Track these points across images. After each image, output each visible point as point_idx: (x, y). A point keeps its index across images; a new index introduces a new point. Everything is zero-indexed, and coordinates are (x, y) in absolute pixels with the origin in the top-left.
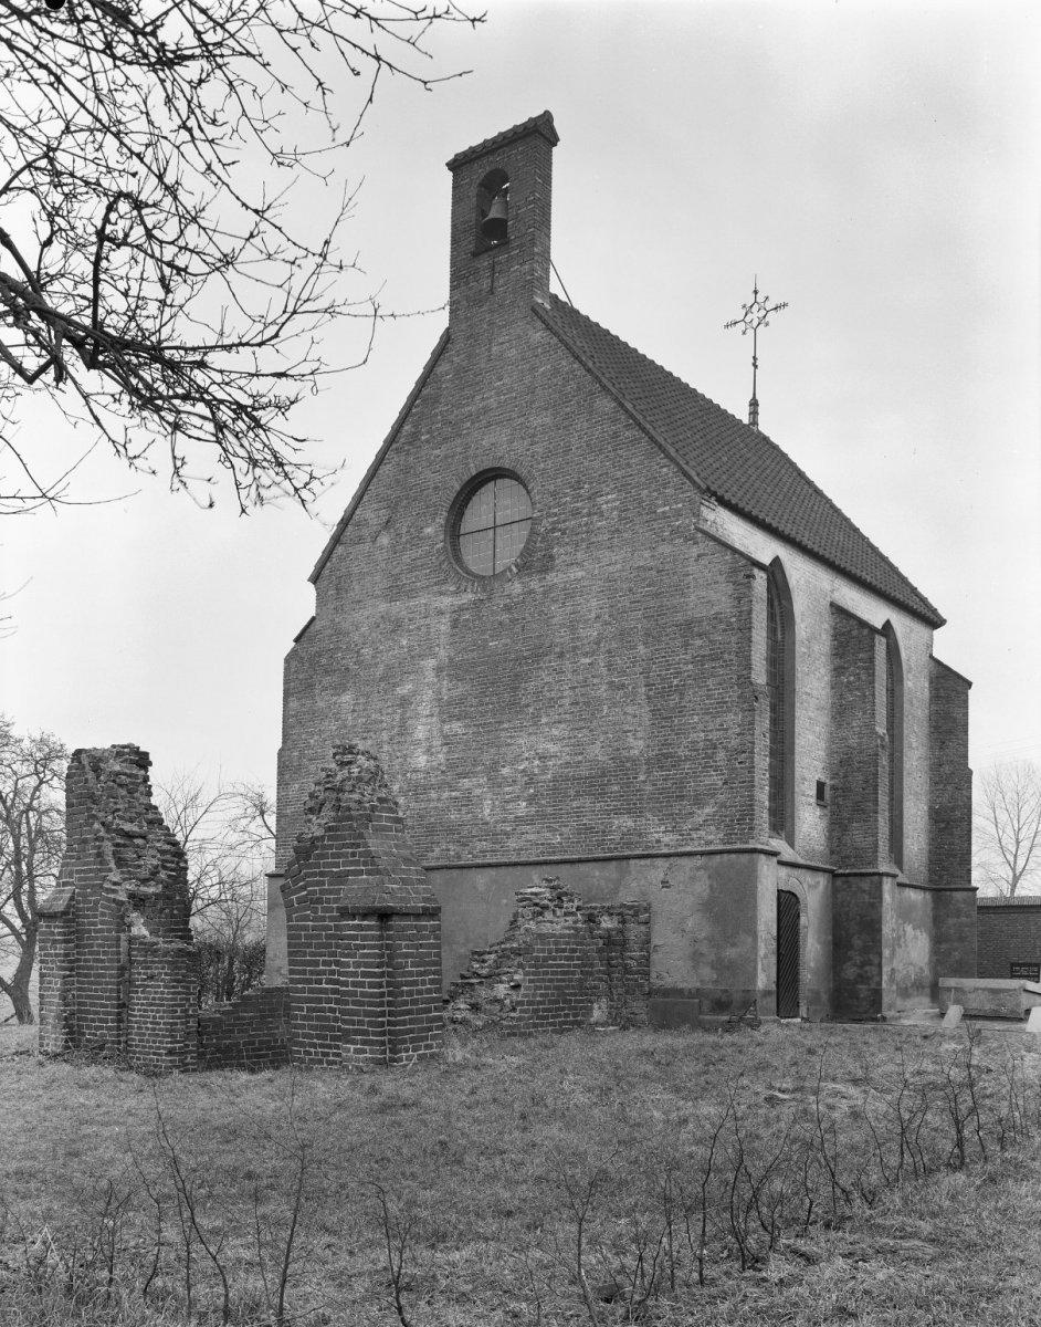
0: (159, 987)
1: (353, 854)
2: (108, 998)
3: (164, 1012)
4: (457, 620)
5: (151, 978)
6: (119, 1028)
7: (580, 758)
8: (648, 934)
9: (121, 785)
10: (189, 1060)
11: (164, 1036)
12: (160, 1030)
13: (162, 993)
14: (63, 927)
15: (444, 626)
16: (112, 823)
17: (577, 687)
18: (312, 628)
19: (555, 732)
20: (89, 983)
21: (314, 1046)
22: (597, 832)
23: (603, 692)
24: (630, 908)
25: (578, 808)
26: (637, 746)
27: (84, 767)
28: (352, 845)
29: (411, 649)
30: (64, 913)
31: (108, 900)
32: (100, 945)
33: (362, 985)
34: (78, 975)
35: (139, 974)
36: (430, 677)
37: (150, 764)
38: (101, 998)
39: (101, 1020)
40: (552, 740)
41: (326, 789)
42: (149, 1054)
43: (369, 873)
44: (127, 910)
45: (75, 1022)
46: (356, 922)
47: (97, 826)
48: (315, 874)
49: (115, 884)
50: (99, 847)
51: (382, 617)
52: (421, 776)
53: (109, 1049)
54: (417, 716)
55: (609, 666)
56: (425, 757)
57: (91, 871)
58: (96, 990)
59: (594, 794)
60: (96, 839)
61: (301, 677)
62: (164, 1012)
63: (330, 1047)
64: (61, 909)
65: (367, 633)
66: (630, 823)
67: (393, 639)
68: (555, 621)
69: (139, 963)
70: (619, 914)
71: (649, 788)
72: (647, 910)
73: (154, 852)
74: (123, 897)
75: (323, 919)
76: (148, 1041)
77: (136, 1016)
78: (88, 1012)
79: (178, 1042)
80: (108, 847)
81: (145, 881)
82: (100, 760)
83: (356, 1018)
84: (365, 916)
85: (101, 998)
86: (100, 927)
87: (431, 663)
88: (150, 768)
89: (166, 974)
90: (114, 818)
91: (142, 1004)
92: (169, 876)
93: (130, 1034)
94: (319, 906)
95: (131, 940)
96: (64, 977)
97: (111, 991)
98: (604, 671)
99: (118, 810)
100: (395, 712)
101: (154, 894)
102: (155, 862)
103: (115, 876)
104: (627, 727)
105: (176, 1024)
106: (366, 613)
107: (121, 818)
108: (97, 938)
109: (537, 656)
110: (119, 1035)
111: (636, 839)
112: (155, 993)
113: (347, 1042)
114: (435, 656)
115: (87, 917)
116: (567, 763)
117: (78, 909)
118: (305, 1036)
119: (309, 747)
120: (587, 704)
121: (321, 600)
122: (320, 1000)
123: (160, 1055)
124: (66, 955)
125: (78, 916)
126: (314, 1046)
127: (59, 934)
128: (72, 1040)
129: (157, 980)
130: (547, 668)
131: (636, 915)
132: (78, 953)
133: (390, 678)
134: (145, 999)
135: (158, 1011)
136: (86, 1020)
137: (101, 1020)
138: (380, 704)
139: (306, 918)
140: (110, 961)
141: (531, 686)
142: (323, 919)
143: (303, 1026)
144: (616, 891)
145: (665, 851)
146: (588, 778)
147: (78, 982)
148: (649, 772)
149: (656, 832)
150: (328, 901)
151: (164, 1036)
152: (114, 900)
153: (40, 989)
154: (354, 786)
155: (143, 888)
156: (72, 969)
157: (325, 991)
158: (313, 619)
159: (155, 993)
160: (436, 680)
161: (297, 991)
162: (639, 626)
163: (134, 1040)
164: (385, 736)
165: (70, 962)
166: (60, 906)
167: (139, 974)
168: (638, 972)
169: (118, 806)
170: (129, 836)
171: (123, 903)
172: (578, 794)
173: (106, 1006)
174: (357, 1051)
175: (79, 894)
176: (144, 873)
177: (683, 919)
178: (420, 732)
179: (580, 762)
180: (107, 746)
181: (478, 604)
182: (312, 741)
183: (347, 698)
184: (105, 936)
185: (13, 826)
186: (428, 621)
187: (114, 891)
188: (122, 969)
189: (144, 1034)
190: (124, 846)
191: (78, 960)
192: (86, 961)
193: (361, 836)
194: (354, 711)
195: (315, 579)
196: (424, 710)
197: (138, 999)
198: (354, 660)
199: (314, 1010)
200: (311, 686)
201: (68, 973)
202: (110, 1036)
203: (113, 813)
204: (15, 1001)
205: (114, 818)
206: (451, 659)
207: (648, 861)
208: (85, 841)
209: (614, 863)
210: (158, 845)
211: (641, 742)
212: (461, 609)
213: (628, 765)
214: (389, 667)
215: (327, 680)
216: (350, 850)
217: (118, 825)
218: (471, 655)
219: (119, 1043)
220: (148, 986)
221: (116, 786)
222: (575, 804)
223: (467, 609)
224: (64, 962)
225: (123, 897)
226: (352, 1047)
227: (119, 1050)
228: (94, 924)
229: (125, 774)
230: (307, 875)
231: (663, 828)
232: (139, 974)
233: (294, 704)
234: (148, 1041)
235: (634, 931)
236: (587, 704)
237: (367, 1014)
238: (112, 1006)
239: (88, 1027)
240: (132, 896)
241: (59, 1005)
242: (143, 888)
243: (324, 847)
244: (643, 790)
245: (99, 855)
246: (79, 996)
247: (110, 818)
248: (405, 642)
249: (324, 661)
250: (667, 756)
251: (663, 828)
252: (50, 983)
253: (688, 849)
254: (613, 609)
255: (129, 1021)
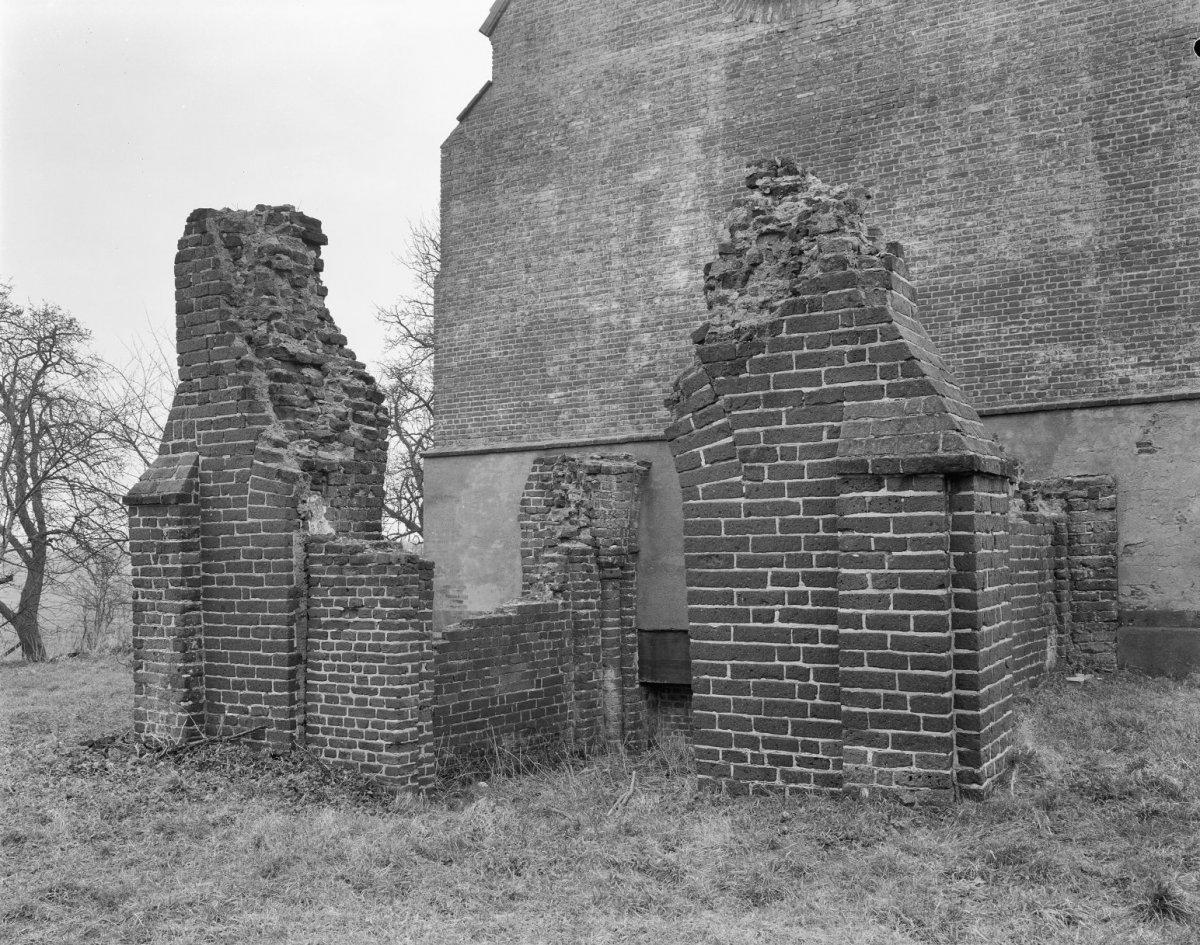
0: (372, 625)
1: (857, 356)
2: (268, 647)
3: (383, 671)
4: (738, 64)
5: (354, 609)
6: (292, 701)
7: (970, 258)
8: (1114, 527)
9: (280, 272)
10: (423, 755)
11: (383, 715)
12: (374, 703)
13: (380, 637)
14: (180, 523)
15: (716, 75)
16: (266, 337)
17: (962, 150)
18: (481, 102)
19: (921, 221)
20: (229, 620)
21: (753, 743)
22: (1003, 372)
23: (1012, 152)
24: (1081, 486)
25: (966, 335)
26: (1080, 234)
27: (211, 240)
28: (853, 337)
29: (656, 114)
30: (182, 498)
31: (267, 472)
32: (250, 554)
33: (900, 623)
34: (207, 606)
35: (328, 603)
36: (693, 152)
37: (324, 240)
38: (255, 646)
39: (254, 686)
40: (916, 233)
41: (762, 235)
42: (351, 745)
43: (896, 391)
44: (301, 490)
45: (203, 688)
46: (883, 492)
47: (239, 342)
48: (754, 402)
49: (278, 444)
50: (246, 380)
51: (606, 72)
52: (677, 300)
53: (271, 736)
54: (670, 213)
55: (1023, 114)
56: (686, 273)
57: (230, 422)
58: (244, 633)
59: (999, 313)
60: (241, 366)
61: (470, 169)
62: (383, 671)
63: (792, 746)
64: (177, 490)
65: (580, 99)
66: (1068, 355)
67: (625, 103)
68: (915, 53)
69: (327, 583)
70: (1061, 496)
71: (1103, 298)
72: (1111, 488)
73: (339, 392)
74: (294, 468)
75: (777, 490)
76: (350, 723)
77: (323, 678)
78: (230, 671)
79: (410, 724)
80: (261, 381)
81: (325, 441)
82: (241, 228)
83: (881, 692)
84: (907, 479)
85: (255, 646)
86: (249, 520)
87: (695, 132)
88: (322, 247)
89: (385, 603)
90: (270, 329)
91: (335, 658)
92: (367, 433)
93: (314, 708)
94: (766, 466)
95: (309, 544)
96: (185, 609)
97: (276, 634)
98: (1015, 122)
99: (278, 315)
100: (631, 210)
101: (342, 463)
102: (342, 409)
103: (276, 431)
104: (1061, 206)
105: (405, 692)
106: (579, 69)
107: (282, 329)
108: (246, 542)
109: (886, 106)
110: (292, 713)
111: (1080, 378)
112: (363, 637)
113: (857, 741)
114: (700, 122)
115: (225, 504)
116: (946, 268)
117: (204, 491)
118: (725, 723)
119: (486, 269)
120: (982, 174)
121: (500, 59)
122: (768, 654)
123: (378, 748)
124: (186, 571)
125: (205, 504)
126: (753, 743)
127: (172, 534)
128: (200, 720)
129: (367, 615)
130: (903, 124)
131: (1093, 496)
132: (206, 568)
133: (621, 161)
134: (340, 647)
135: (369, 670)
136: (224, 684)
137: (254, 686)
138: (605, 200)
139: (734, 490)
140: (271, 580)
141: (875, 155)
142: (777, 490)
143: (723, 705)
144: (1048, 461)
145: (1138, 395)
146: (986, 288)
147: (208, 618)
148: (1103, 273)
149: (1121, 367)
150: (789, 454)
151: (383, 715)
152: (279, 474)
153: (135, 632)
154: (840, 220)
155: (322, 453)
156: (196, 597)
157: (783, 635)
158: (489, 85)
159: (363, 637)
160: (702, 157)
161: (708, 634)
162: (1081, 47)
163: (321, 721)
164: (615, 245)
165: (193, 583)
166: (174, 484)
167: (327, 604)
168: (1097, 587)
169: (277, 308)
170: (296, 362)
171: (290, 478)
172: (966, 315)
173: (267, 661)
174: (880, 760)
175: (206, 465)
176: (323, 428)
177: (1182, 500)
178: (677, 236)
179: (971, 264)
180: (250, 207)
181: (774, 39)
182: (490, 261)
183: (548, 194)
184: (262, 537)
185: (15, 414)
186: (686, 71)
187: (277, 458)
188: (295, 594)
189: (342, 711)
190: (288, 379)
191: (206, 580)
192: (222, 581)
193: (880, 315)
194: (560, 212)
195: (490, 29)
196: (682, 202)
197: (327, 650)
198: (559, 138)
199: (751, 672)
200: (487, 182)
201: (189, 603)
202: (275, 713)
203: (268, 320)
204: (21, 631)
205: (270, 329)
206: (728, 124)
207: (1110, 412)
208: (218, 371)
209: (1043, 418)
210: (344, 379)
211: (1088, 229)
212: (745, 48)
213: (1063, 264)
214: (619, 145)
215: (514, 171)
216: (848, 348)
217: (277, 341)
218: (764, 115)
219: (293, 726)
220: (348, 625)
221: (272, 273)
222: (961, 330)
223: (756, 48)
224: (182, 584)
225: (294, 468)
226: (870, 752)
227: (292, 737)
228: (241, 516)
229: (287, 253)
230: (733, 404)
231: (1133, 360)
232: (328, 603)
233: (459, 210)
234: (350, 723)
235: (1088, 522)
236: (982, 174)
237: (909, 683)
238: (279, 661)
239: (230, 698)
240: (308, 466)
241: (173, 659)
242: (322, 453)
243: (778, 345)
244: (1094, 302)
245: (247, 393)
246: (209, 644)
247: (263, 329)
248: (646, 106)
249: (507, 144)
250: (1136, 247)
251: (1133, 360)
252: (156, 620)
253: (1186, 390)
254: (1028, 25)
255: (308, 687)
